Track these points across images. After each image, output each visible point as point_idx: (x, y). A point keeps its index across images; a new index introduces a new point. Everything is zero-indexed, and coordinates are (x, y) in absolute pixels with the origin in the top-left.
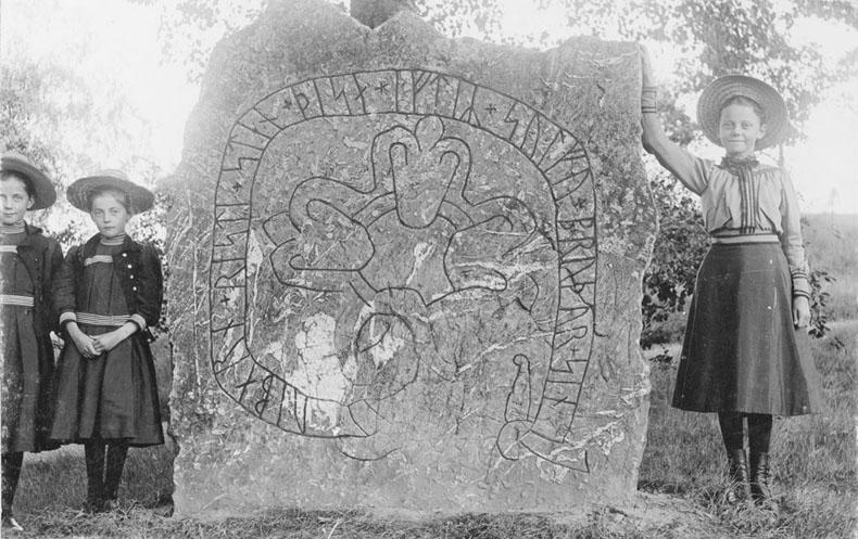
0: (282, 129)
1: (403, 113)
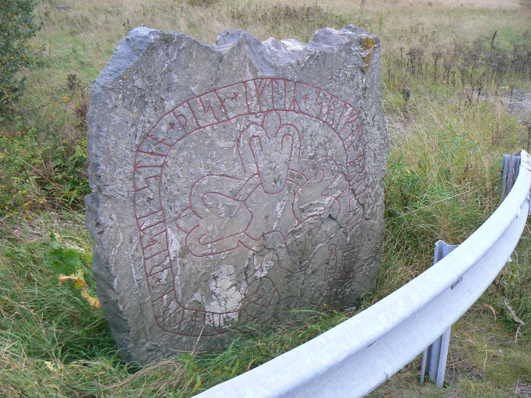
0: (172, 146)
1: (254, 113)
